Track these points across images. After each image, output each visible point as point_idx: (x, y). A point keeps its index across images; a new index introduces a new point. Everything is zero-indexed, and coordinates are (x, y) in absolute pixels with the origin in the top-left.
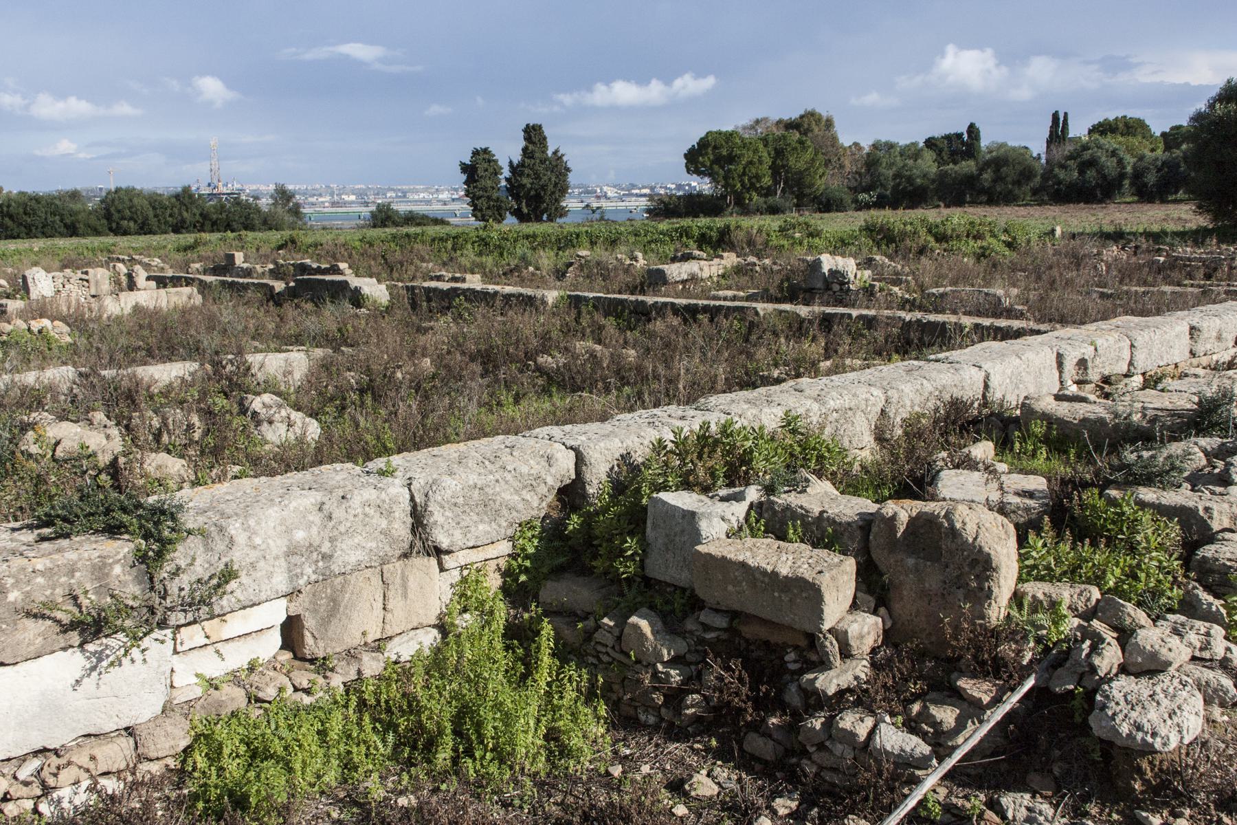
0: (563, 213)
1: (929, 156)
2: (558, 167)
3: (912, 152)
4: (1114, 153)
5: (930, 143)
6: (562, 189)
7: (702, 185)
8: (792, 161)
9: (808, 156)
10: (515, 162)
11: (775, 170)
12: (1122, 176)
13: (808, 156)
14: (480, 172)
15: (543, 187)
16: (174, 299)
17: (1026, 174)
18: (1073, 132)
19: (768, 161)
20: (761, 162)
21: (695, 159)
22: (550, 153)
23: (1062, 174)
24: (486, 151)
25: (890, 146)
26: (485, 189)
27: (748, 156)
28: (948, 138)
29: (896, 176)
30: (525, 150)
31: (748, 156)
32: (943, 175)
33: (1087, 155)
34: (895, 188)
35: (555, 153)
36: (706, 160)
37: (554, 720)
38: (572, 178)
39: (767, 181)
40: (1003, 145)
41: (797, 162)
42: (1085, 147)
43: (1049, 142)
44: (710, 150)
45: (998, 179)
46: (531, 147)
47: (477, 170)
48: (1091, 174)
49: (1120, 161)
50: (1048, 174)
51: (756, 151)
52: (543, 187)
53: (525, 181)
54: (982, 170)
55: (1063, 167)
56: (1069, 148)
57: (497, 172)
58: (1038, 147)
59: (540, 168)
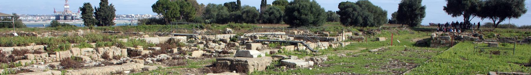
0: (113, 24)
1: (226, 9)
2: (112, 9)
3: (220, 7)
4: (278, 10)
5: (226, 4)
6: (113, 16)
7: (156, 16)
8: (185, 10)
9: (191, 7)
10: (97, 8)
11: (181, 12)
12: (281, 17)
13: (191, 7)
14: (87, 11)
15: (108, 16)
16: (161, 40)
17: (255, 15)
18: (268, 3)
19: (179, 9)
20: (177, 9)
21: (155, 8)
22: (109, 5)
23: (265, 16)
24: (89, 4)
25: (214, 5)
26: (89, 16)
27: (173, 7)
28: (231, 3)
29: (217, 15)
30: (100, 4)
31: (173, 7)
32: (231, 15)
33: (271, 11)
34: (217, 18)
35: (111, 5)
36: (160, 9)
37: (362, 16)
38: (116, 13)
39: (178, 15)
40: (248, 6)
41: (186, 10)
42: (271, 9)
43: (261, 6)
44: (161, 5)
45: (248, 16)
46: (103, 3)
47: (85, 10)
48: (272, 16)
49: (280, 13)
50: (261, 16)
51: (175, 6)
52: (108, 16)
53: (102, 14)
54: (243, 13)
55: (265, 14)
56: (267, 8)
57: (92, 10)
58: (258, 7)
59: (106, 10)
